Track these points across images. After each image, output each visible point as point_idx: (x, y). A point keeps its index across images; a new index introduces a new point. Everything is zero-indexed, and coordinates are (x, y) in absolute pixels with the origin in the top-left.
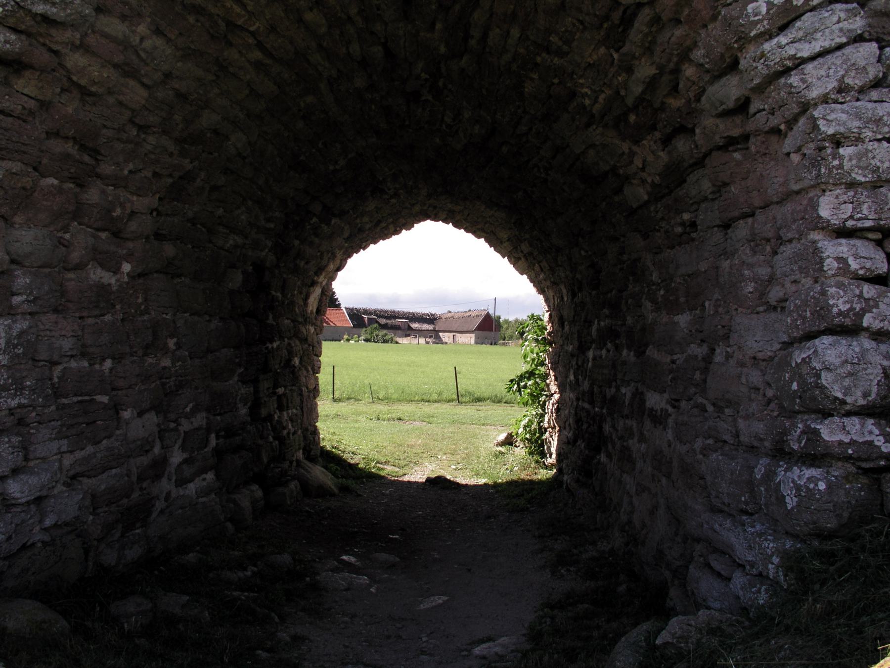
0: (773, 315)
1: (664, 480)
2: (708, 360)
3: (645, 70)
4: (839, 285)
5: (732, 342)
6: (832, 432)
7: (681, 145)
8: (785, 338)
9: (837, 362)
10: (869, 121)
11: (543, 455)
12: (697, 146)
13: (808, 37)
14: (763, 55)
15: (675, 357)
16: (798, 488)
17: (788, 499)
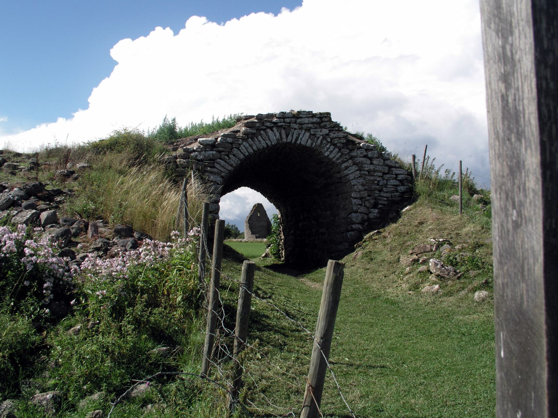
13: (350, 171)
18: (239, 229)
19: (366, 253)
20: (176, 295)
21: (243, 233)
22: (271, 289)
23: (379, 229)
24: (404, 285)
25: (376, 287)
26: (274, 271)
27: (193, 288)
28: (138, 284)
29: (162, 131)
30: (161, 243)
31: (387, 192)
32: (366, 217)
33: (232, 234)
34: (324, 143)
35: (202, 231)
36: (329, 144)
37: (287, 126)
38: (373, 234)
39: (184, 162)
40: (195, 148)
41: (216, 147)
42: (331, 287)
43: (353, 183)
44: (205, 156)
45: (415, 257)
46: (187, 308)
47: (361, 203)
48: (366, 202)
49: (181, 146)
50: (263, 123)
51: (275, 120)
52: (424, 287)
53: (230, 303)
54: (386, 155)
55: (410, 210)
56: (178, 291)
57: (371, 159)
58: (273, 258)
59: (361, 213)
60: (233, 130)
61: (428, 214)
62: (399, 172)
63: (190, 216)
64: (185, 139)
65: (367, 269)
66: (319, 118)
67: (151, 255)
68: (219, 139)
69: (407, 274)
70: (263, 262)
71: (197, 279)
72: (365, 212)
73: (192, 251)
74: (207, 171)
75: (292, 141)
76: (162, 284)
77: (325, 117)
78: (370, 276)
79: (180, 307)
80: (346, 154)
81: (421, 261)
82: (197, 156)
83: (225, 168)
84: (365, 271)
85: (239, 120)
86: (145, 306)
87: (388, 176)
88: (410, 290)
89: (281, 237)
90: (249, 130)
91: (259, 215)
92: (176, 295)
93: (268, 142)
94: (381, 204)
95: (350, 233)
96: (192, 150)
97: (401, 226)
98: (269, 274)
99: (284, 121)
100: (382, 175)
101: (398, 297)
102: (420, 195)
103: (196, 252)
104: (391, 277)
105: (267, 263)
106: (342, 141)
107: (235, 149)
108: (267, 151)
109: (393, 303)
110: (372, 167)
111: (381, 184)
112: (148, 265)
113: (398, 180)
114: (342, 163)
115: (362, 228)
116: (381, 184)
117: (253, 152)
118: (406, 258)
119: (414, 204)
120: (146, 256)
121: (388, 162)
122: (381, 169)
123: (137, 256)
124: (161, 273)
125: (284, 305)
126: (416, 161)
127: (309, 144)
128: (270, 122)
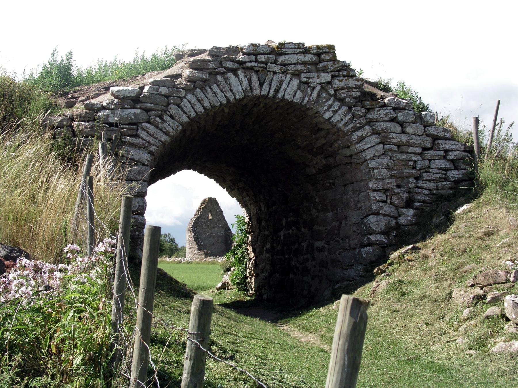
0: (359, 211)
1: (324, 270)
2: (340, 226)
3: (323, 141)
4: (374, 203)
5: (347, 219)
6: (373, 238)
7: (331, 160)
8: (362, 217)
9: (374, 221)
10: (381, 164)
11: (247, 290)
12: (336, 162)
13: (366, 144)
14: (356, 148)
15: (327, 228)
16: (366, 252)
17: (364, 255)
18: (176, 241)
19: (394, 284)
20: (72, 355)
21: (183, 248)
22: (233, 343)
23: (416, 242)
24: (459, 340)
25: (411, 342)
26: (238, 313)
27: (102, 341)
28: (5, 336)
29: (46, 73)
30: (47, 264)
31: (429, 181)
32: (393, 223)
33: (164, 250)
34: (324, 98)
35: (119, 245)
36: (332, 99)
37: (262, 67)
38: (406, 252)
39: (86, 127)
40: (105, 104)
41: (141, 102)
42: (346, 341)
43: (372, 164)
44: (121, 118)
45: (478, 291)
46: (92, 376)
47: (385, 199)
48: (394, 198)
49: (80, 99)
50: (221, 63)
51: (241, 57)
52: (495, 343)
53: (164, 367)
54: (428, 118)
55: (470, 211)
56: (76, 346)
57: (402, 124)
58: (234, 290)
59: (384, 215)
60: (170, 74)
61: (501, 218)
62: (450, 147)
63: (96, 218)
64: (87, 87)
65: (394, 311)
66: (314, 54)
67: (29, 285)
68: (146, 89)
69: (465, 321)
70: (217, 297)
71: (109, 326)
72: (392, 214)
73: (101, 278)
74: (125, 143)
75: (269, 93)
76: (48, 336)
77: (326, 53)
78: (401, 323)
79: (79, 374)
80: (361, 116)
81: (489, 299)
82: (107, 116)
83: (156, 138)
84: (393, 314)
85: (180, 56)
86: (17, 374)
87: (432, 153)
88: (471, 349)
89: (248, 254)
90: (197, 74)
91: (210, 217)
92: (72, 355)
93: (229, 95)
94: (420, 201)
95: (366, 249)
96: (99, 106)
97: (454, 237)
98: (229, 318)
99: (256, 59)
100: (420, 152)
101: (449, 359)
102: (486, 185)
103: (109, 280)
104: (437, 325)
105: (226, 300)
106: (353, 94)
107: (173, 106)
108: (226, 110)
109: (442, 370)
110: (404, 138)
111: (419, 166)
112: (25, 302)
113: (449, 160)
114: (354, 132)
115: (386, 242)
116: (419, 166)
117: (203, 110)
118: (462, 292)
119: (476, 201)
120: (19, 288)
121: (431, 130)
122: (419, 141)
123: (5, 288)
124: (47, 316)
125: (256, 371)
126: (480, 127)
127: (297, 99)
128: (233, 61)
